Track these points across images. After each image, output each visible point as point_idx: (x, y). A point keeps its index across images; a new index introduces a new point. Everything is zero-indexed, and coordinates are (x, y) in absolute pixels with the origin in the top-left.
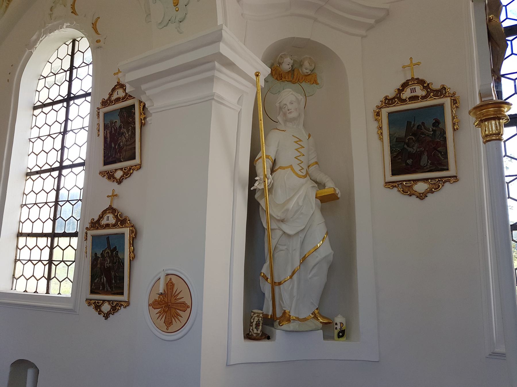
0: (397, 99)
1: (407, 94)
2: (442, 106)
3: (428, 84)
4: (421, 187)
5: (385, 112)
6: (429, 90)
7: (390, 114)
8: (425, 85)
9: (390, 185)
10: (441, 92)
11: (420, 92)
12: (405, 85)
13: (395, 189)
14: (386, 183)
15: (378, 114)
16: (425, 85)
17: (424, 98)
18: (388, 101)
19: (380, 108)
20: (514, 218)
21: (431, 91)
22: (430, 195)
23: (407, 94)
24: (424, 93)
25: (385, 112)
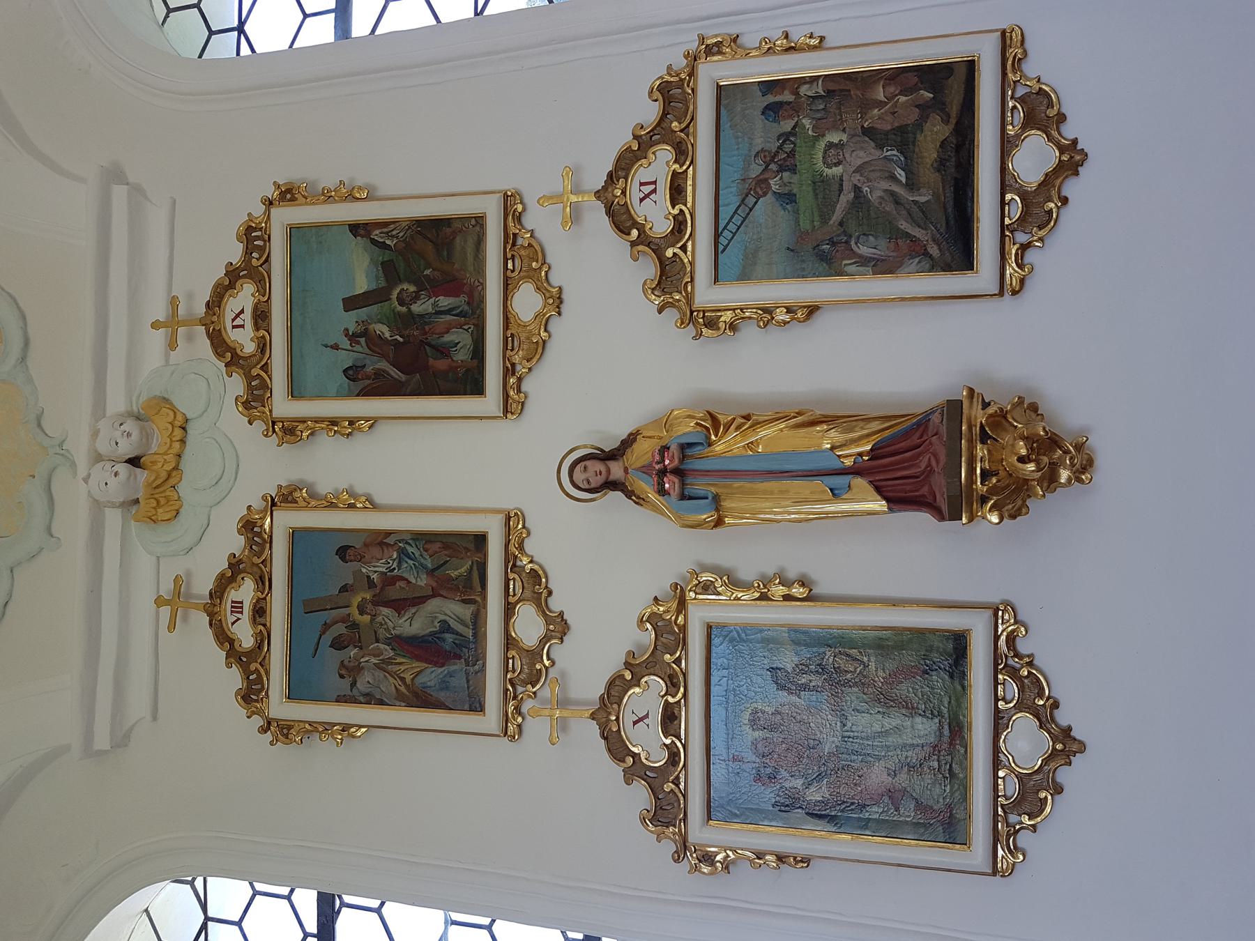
12: (617, 747)
21: (250, 267)
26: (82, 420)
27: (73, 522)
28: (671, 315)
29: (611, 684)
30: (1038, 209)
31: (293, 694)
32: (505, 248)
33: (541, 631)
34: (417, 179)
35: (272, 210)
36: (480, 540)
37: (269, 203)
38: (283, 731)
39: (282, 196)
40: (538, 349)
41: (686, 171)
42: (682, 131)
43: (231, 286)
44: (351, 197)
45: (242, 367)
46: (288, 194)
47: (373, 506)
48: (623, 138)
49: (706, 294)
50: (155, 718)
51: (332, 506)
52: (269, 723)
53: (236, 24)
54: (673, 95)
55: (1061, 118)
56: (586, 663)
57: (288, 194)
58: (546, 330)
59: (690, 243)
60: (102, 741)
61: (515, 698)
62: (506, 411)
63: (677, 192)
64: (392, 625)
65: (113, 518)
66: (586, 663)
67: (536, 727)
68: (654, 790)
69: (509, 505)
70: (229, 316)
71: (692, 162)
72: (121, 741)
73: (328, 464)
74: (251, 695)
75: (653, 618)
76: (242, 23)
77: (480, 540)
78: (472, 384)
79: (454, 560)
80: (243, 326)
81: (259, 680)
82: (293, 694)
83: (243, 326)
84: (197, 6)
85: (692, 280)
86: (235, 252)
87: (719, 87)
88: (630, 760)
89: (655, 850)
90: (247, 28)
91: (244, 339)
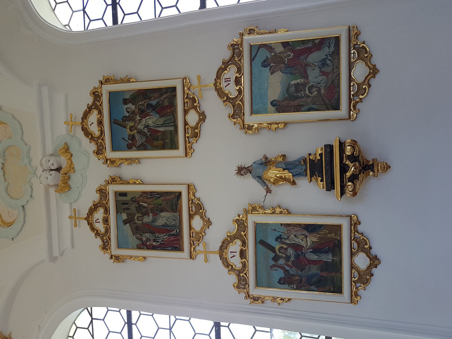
0: (98, 140)
1: (236, 262)
2: (257, 226)
3: (228, 236)
4: (362, 261)
5: (110, 154)
6: (94, 107)
7: (258, 284)
8: (229, 239)
9: (354, 297)
10: (96, 95)
11: (236, 246)
12: (227, 264)
13: (194, 146)
14: (352, 302)
15: (256, 299)
16: (229, 239)
17: (244, 243)
18: (242, 284)
19: (248, 296)
20: (195, 6)
21: (96, 106)
22: (374, 251)
23: (94, 129)
24: (239, 242)
25: (110, 154)
26: (40, 154)
27: (39, 190)
28: (238, 126)
29: (223, 242)
30: (364, 278)
31: (119, 246)
32: (189, 203)
33: (201, 225)
34: (150, 73)
35: (103, 86)
36: (174, 89)
37: (102, 83)
38: (117, 259)
39: (106, 81)
40: (196, 136)
41: (241, 77)
42: (239, 60)
43: (90, 111)
44: (128, 81)
45: (94, 140)
46: (107, 81)
47: (142, 183)
48: (219, 64)
49: (250, 119)
50: (73, 247)
51: (128, 183)
52: (107, 160)
53: (81, 8)
54: (236, 49)
55: (370, 248)
56: (214, 237)
57: (107, 81)
58: (204, 232)
59: (242, 76)
60: (56, 253)
61: (194, 245)
62: (186, 156)
63: (238, 81)
64: (152, 223)
65: (52, 191)
66: (214, 237)
67: (201, 257)
68: (238, 275)
69: (189, 182)
70: (95, 219)
71: (243, 74)
72: (62, 254)
73: (127, 171)
74: (105, 246)
75: (237, 221)
76: (84, 8)
77: (174, 89)
78: (174, 146)
79: (171, 201)
80: (99, 222)
81: (107, 242)
82: (119, 246)
83: (99, 222)
84: (67, 2)
85: (244, 115)
86: (90, 100)
87: (251, 46)
88: (230, 267)
89: (239, 297)
90: (86, 10)
91: (101, 227)
